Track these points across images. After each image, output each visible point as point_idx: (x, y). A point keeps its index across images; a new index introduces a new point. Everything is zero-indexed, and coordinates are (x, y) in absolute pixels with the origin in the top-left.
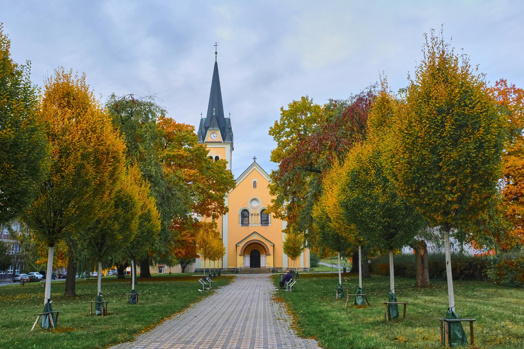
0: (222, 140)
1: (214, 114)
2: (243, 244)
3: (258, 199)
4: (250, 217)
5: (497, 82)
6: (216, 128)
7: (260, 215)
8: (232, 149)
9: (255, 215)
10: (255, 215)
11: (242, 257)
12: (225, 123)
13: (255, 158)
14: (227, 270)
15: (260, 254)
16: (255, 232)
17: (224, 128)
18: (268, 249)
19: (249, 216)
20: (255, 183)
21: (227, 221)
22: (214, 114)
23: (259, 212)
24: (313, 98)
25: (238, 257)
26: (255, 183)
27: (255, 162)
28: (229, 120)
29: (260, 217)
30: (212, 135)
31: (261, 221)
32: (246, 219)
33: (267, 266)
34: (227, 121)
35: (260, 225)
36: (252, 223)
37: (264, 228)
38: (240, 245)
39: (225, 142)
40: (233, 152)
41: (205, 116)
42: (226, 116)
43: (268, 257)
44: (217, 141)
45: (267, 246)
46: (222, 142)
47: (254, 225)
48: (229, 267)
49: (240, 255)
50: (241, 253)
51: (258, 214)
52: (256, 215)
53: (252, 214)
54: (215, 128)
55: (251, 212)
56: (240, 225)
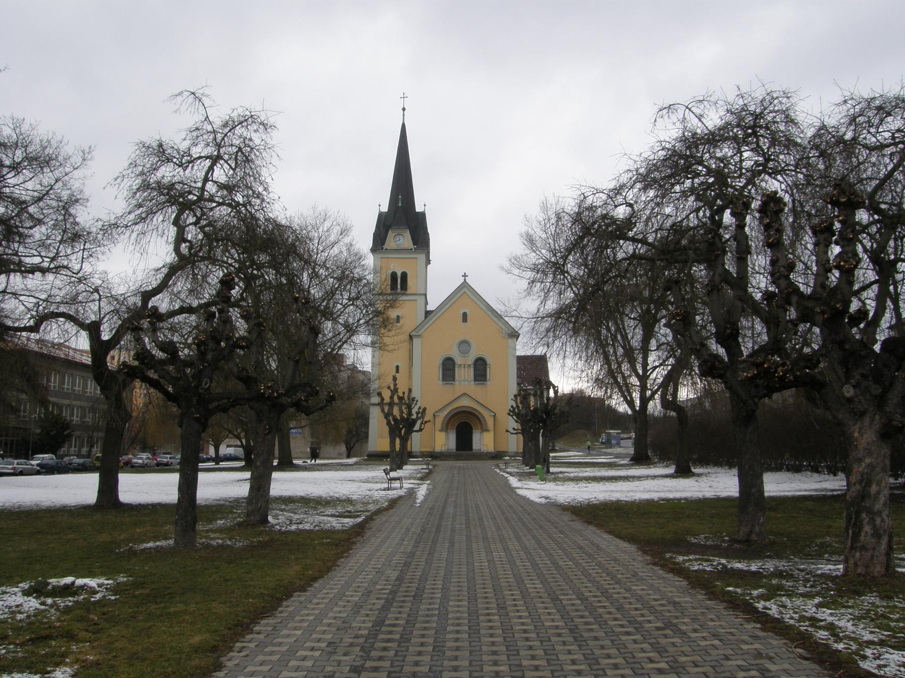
1: (400, 204)
20: (465, 315)
22: (400, 204)
26: (465, 315)
27: (465, 280)
40: (429, 266)
41: (385, 209)
42: (419, 208)
48: (423, 450)
50: (442, 427)
53: (460, 365)
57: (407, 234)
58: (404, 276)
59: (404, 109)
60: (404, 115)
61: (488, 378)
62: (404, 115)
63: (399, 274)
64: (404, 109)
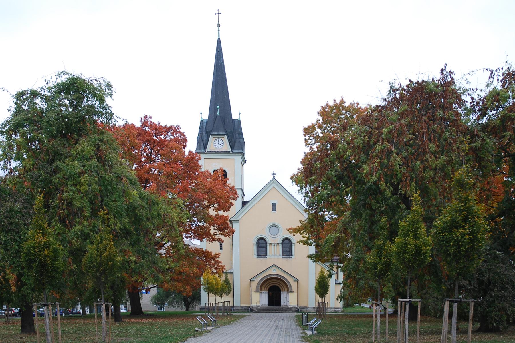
0: (230, 149)
1: (218, 113)
6: (221, 133)
8: (244, 161)
20: (274, 205)
22: (218, 113)
26: (274, 205)
40: (245, 165)
41: (206, 116)
42: (235, 116)
46: (230, 152)
57: (225, 139)
60: (219, 31)
62: (219, 31)
64: (219, 25)
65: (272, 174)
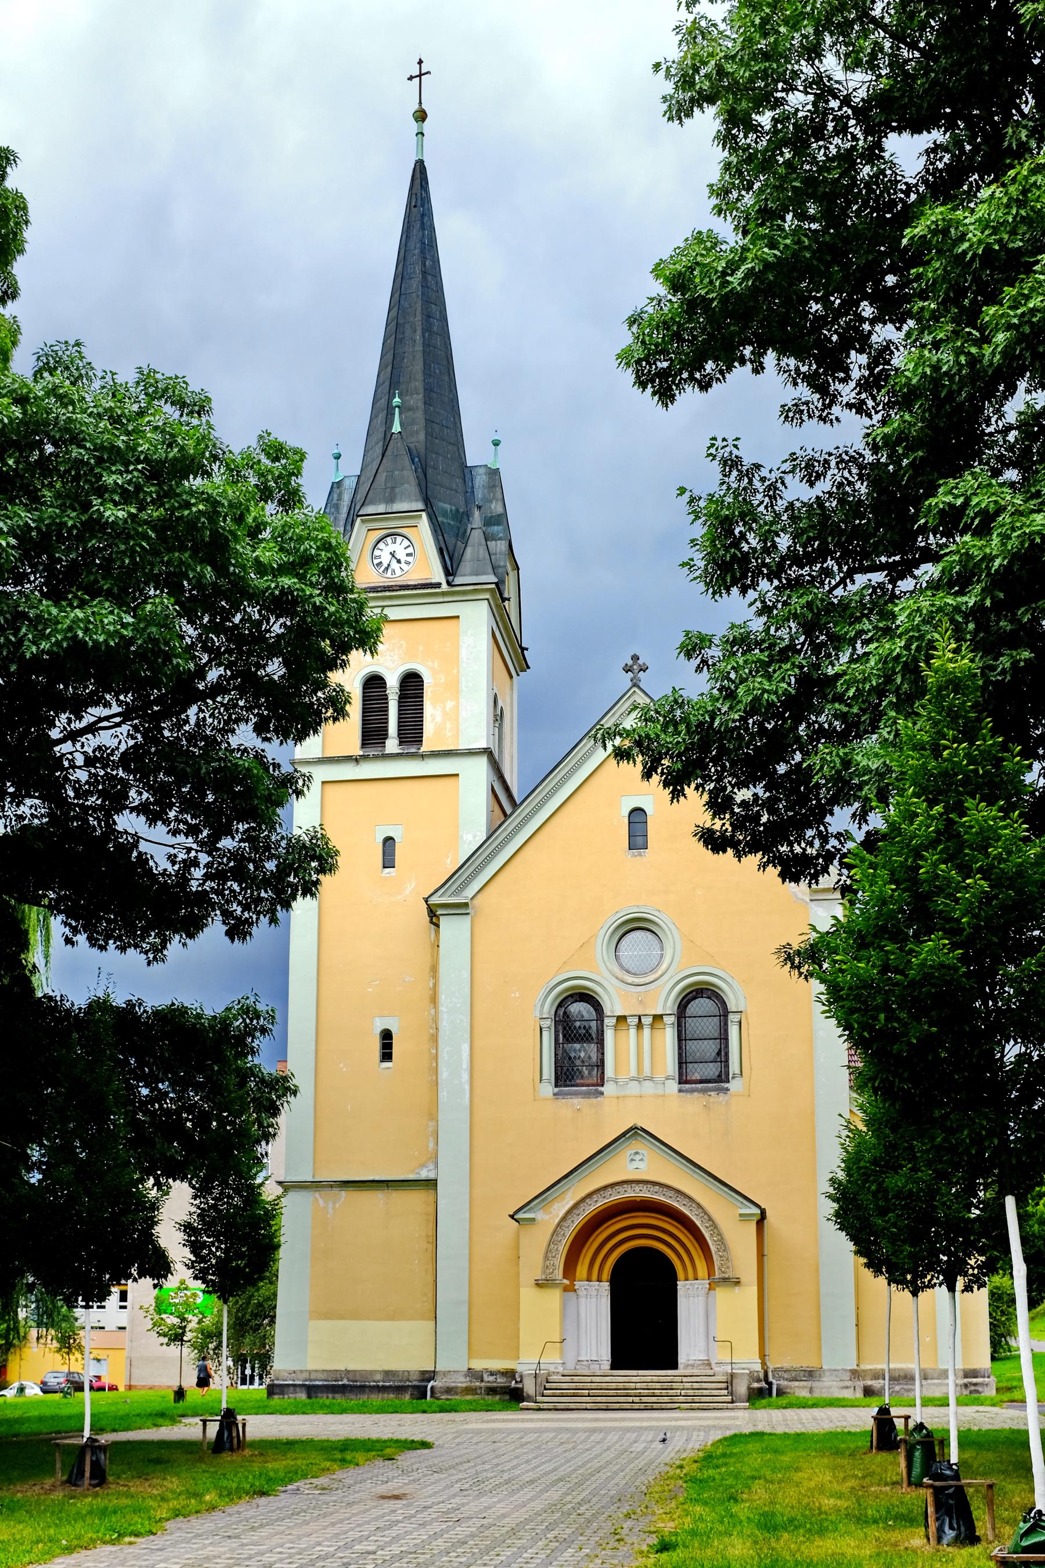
2: (560, 1208)
3: (663, 919)
4: (609, 1035)
5: (644, 669)
7: (670, 1020)
9: (640, 1026)
10: (640, 1026)
11: (554, 1296)
12: (469, 493)
13: (682, 491)
14: (461, 1382)
15: (673, 1278)
16: (634, 1132)
17: (462, 517)
18: (722, 1241)
19: (601, 1033)
21: (465, 1064)
23: (664, 1002)
24: (633, 860)
25: (528, 1294)
28: (494, 474)
29: (669, 1036)
30: (384, 553)
31: (683, 1062)
32: (584, 1051)
33: (722, 1362)
34: (480, 480)
35: (673, 1086)
36: (623, 1077)
37: (694, 1104)
38: (539, 1215)
39: (458, 580)
40: (416, 107)
43: (722, 1294)
44: (414, 578)
45: (714, 1226)
47: (634, 1088)
49: (539, 1285)
51: (658, 1018)
52: (647, 1021)
53: (621, 1019)
54: (398, 506)
55: (614, 1004)
56: (548, 1089)
58: (412, 683)
59: (421, 116)
61: (734, 1067)
63: (393, 683)
65: (627, 669)
